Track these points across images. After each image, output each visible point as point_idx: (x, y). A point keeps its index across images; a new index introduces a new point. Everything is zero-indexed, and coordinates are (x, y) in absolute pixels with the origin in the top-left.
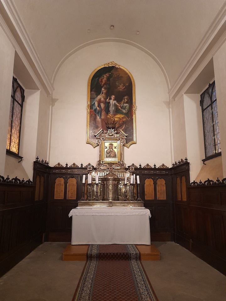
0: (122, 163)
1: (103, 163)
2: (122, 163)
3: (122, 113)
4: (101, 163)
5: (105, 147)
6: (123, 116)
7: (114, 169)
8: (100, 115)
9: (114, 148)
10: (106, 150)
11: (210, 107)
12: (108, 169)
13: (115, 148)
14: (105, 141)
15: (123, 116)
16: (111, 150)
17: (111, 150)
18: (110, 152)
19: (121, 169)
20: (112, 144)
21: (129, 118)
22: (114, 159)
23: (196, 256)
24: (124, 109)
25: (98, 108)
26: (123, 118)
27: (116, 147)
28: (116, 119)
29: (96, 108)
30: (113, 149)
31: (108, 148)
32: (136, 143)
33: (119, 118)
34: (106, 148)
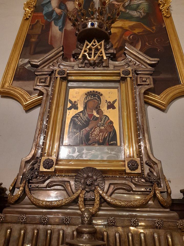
0: (147, 171)
1: (52, 170)
2: (147, 171)
3: (130, 18)
4: (42, 169)
5: (69, 105)
6: (132, 23)
7: (109, 204)
8: (60, 23)
9: (104, 108)
10: (71, 113)
11: (64, 189)
12: (75, 202)
13: (111, 106)
14: (70, 84)
15: (132, 23)
16: (95, 113)
17: (95, 113)
18: (87, 124)
19: (144, 205)
20: (97, 96)
21: (154, 28)
22: (106, 149)
23: (41, 31)
24: (136, 10)
25: (58, 11)
26: (132, 28)
27: (116, 105)
28: (113, 31)
29: (53, 11)
30: (99, 111)
31: (81, 109)
32: (163, 110)
33: (121, 28)
34: (74, 106)
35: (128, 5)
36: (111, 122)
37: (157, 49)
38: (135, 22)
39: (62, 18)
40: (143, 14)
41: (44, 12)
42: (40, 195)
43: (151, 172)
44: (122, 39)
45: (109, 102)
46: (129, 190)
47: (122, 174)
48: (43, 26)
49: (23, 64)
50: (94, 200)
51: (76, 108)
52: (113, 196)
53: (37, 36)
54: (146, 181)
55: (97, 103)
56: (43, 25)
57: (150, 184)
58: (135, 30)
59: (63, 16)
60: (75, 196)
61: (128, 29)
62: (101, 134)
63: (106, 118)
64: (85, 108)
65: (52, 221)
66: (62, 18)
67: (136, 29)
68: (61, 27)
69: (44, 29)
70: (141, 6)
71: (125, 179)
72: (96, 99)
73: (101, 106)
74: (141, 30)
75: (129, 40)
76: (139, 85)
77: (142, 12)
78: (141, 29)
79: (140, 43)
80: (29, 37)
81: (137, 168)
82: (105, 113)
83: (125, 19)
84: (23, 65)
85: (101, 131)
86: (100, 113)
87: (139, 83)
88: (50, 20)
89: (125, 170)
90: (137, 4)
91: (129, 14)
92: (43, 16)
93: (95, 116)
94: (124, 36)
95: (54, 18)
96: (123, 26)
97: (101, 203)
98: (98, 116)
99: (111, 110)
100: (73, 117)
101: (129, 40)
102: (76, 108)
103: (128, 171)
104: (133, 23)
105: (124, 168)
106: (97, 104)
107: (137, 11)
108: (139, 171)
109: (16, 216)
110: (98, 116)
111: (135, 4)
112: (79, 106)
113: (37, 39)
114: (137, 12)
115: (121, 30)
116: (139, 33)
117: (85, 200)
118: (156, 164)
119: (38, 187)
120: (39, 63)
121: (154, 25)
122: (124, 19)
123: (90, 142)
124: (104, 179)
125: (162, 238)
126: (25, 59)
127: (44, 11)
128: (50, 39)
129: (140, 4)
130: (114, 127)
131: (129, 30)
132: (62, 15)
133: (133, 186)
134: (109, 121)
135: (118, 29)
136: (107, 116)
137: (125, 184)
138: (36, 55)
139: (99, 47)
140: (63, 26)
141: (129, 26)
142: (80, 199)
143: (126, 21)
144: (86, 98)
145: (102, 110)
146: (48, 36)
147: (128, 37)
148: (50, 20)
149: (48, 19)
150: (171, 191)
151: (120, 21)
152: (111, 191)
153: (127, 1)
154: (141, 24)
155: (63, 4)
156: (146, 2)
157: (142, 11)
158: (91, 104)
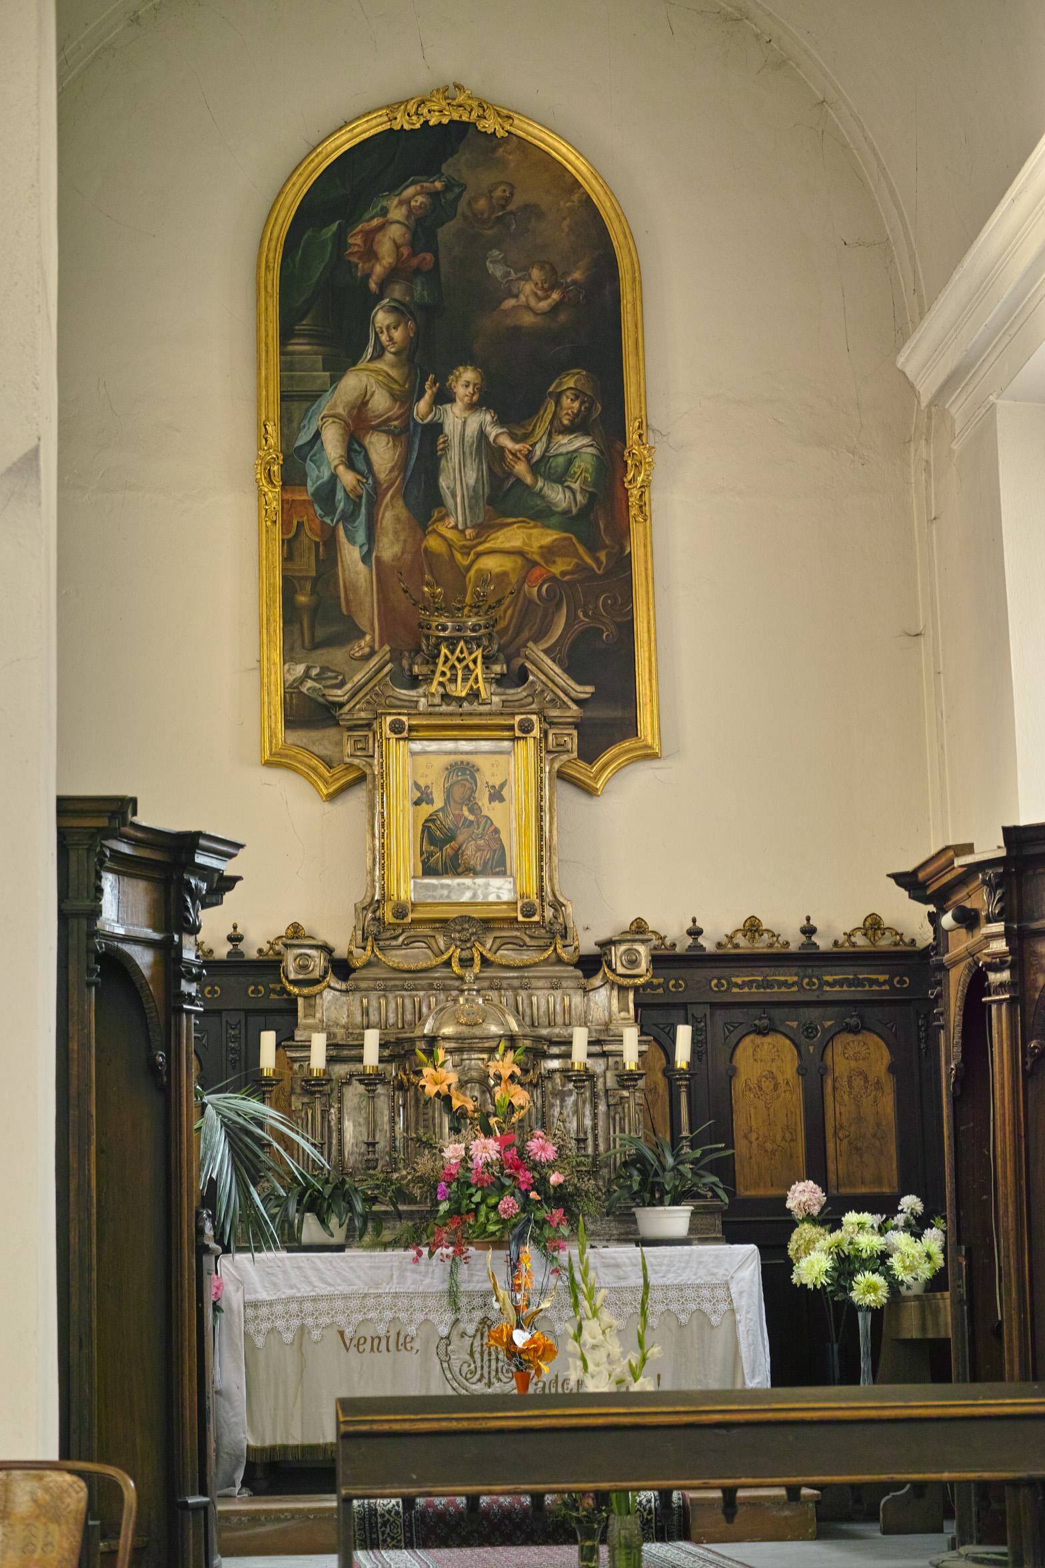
1: (408, 920)
3: (542, 514)
6: (549, 537)
9: (483, 800)
15: (549, 537)
17: (466, 812)
21: (602, 556)
24: (560, 479)
25: (348, 478)
26: (549, 553)
29: (334, 477)
31: (439, 803)
33: (520, 553)
35: (543, 457)
36: (497, 831)
37: (603, 632)
38: (555, 532)
39: (363, 510)
40: (579, 497)
41: (311, 488)
42: (284, 964)
43: (555, 917)
44: (521, 596)
45: (493, 787)
46: (522, 946)
47: (511, 923)
48: (317, 544)
49: (294, 681)
50: (472, 959)
51: (430, 801)
52: (498, 954)
53: (308, 586)
54: (547, 932)
55: (469, 788)
56: (317, 540)
57: (551, 935)
58: (554, 562)
59: (364, 500)
60: (445, 957)
61: (537, 558)
62: (479, 854)
63: (486, 822)
64: (447, 800)
65: (419, 987)
66: (363, 510)
67: (559, 560)
68: (365, 548)
69: (321, 558)
70: (577, 463)
71: (517, 929)
72: (467, 780)
73: (476, 795)
74: (502, 956)
75: (538, 602)
76: (549, 752)
77: (579, 490)
78: (568, 560)
79: (564, 611)
80: (289, 587)
81: (533, 915)
82: (485, 812)
83: (532, 519)
84: (295, 685)
85: (479, 849)
86: (476, 812)
87: (551, 748)
88: (332, 521)
89: (516, 918)
90: (568, 453)
91: (543, 497)
92: (311, 503)
93: (466, 819)
94: (526, 585)
95: (343, 511)
96: (526, 548)
97: (482, 963)
98: (471, 817)
99: (496, 804)
100: (426, 821)
101: (538, 602)
102: (430, 801)
103: (520, 918)
104: (552, 535)
105: (513, 915)
106: (469, 792)
107: (566, 484)
108: (536, 918)
109: (89, 1072)
110: (471, 817)
111: (561, 454)
112: (435, 796)
113: (312, 594)
114: (566, 490)
115: (519, 560)
116: (564, 574)
117: (460, 960)
118: (564, 905)
119: (389, 946)
120: (346, 697)
121: (606, 546)
122: (528, 521)
123: (460, 870)
124: (488, 930)
125: (558, 1000)
126: (297, 664)
127: (309, 483)
128: (342, 595)
129: (575, 455)
130: (501, 840)
131: (542, 563)
132: (360, 497)
133: (527, 939)
134: (492, 828)
135: (513, 558)
136: (488, 818)
137: (516, 937)
138: (319, 652)
139: (472, 666)
140: (369, 544)
141: (541, 547)
142: (453, 960)
143: (535, 527)
144: (447, 778)
145: (480, 804)
146: (337, 584)
147: (536, 589)
148: (332, 521)
149: (326, 514)
150: (200, 925)
151: (518, 527)
152: (495, 948)
153: (541, 438)
154: (571, 539)
155: (358, 449)
156: (591, 445)
157: (576, 486)
158: (458, 793)
